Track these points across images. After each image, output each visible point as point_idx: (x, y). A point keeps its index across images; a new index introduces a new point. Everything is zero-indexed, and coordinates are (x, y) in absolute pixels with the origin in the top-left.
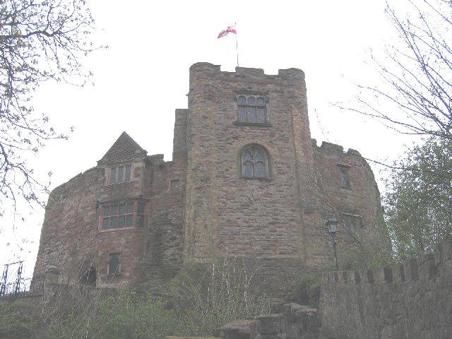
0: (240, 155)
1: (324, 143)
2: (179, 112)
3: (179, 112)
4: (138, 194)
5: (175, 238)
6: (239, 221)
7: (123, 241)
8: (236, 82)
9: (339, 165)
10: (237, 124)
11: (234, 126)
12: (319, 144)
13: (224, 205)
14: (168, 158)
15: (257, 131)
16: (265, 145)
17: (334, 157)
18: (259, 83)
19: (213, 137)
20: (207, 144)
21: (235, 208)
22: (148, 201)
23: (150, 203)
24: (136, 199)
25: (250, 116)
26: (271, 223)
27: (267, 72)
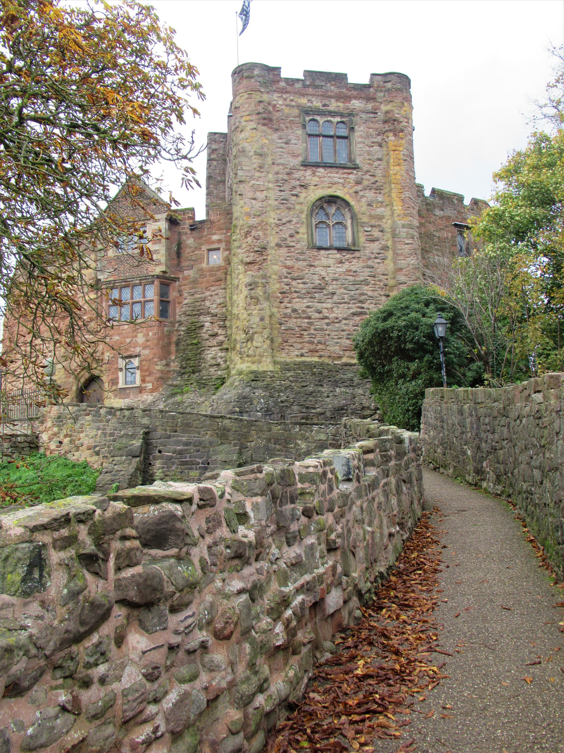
0: (311, 213)
1: (434, 191)
2: (278, 69)
3: (278, 69)
4: (158, 270)
5: (215, 335)
6: (309, 310)
7: (140, 339)
8: (303, 95)
9: (456, 225)
10: (306, 165)
11: (302, 168)
12: (427, 193)
13: (287, 287)
14: (201, 215)
15: (336, 176)
16: (347, 198)
17: (449, 212)
18: (339, 97)
19: (271, 185)
20: (259, 195)
21: (304, 291)
22: (175, 280)
23: (177, 283)
24: (158, 277)
25: (326, 150)
26: (354, 314)
27: (352, 79)
